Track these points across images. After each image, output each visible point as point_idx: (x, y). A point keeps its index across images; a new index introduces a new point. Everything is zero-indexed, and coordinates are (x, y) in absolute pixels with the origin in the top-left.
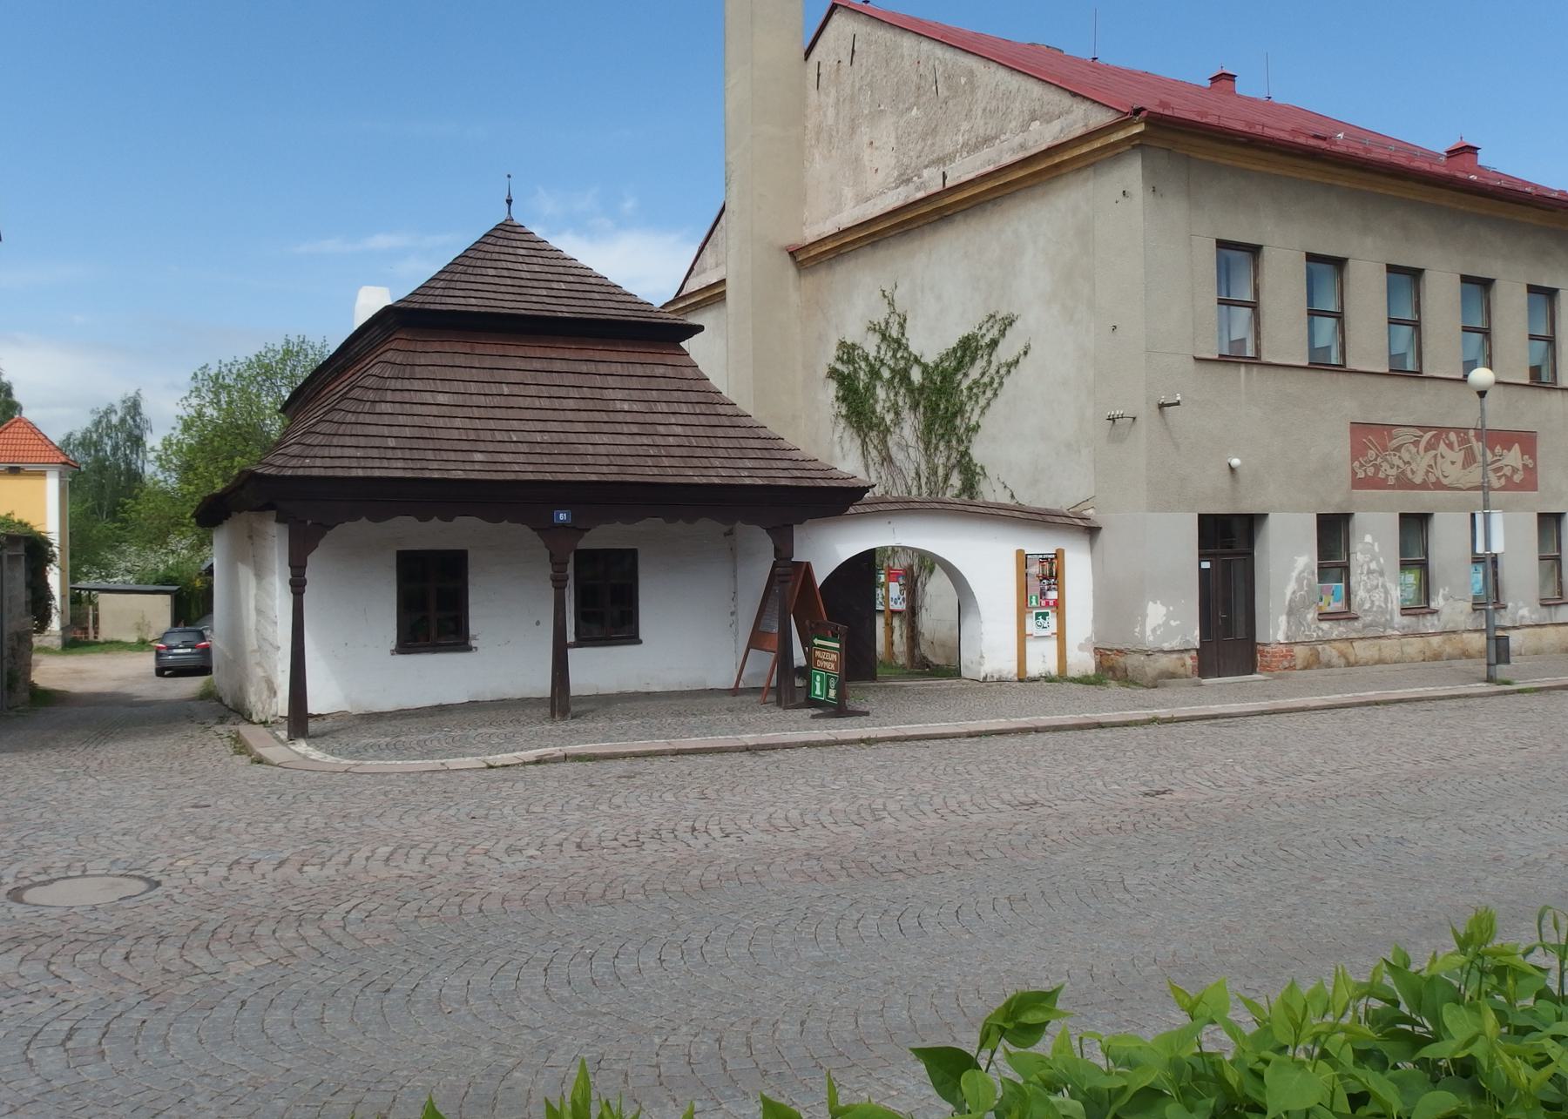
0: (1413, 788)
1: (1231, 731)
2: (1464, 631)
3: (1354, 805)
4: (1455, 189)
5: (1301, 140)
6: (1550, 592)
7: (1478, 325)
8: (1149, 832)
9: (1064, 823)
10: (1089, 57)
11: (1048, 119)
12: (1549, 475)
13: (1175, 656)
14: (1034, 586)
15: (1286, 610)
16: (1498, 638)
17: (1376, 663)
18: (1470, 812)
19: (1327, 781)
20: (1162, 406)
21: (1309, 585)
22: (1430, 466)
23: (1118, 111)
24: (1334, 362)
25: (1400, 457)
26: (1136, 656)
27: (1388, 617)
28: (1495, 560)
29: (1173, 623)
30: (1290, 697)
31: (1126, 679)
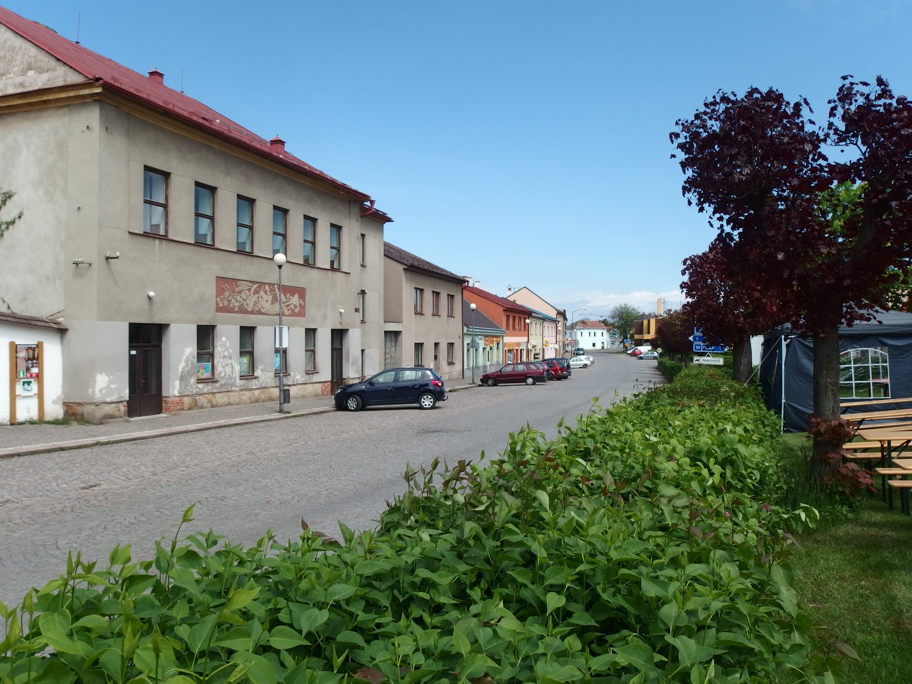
0: (235, 469)
1: (144, 447)
2: (270, 387)
3: (203, 482)
4: (271, 160)
5: (195, 118)
6: (310, 368)
7: (281, 232)
8: (81, 511)
9: (25, 512)
10: (74, 40)
11: (40, 71)
12: (311, 310)
13: (113, 405)
14: (22, 365)
15: (179, 377)
16: (285, 390)
17: (227, 405)
18: (260, 479)
19: (191, 470)
20: (108, 258)
21: (192, 364)
22: (256, 302)
23: (86, 76)
24: (247, 250)
25: (241, 297)
26: (90, 406)
27: (233, 381)
28: (285, 351)
29: (113, 386)
30: (180, 425)
31: (83, 420)
